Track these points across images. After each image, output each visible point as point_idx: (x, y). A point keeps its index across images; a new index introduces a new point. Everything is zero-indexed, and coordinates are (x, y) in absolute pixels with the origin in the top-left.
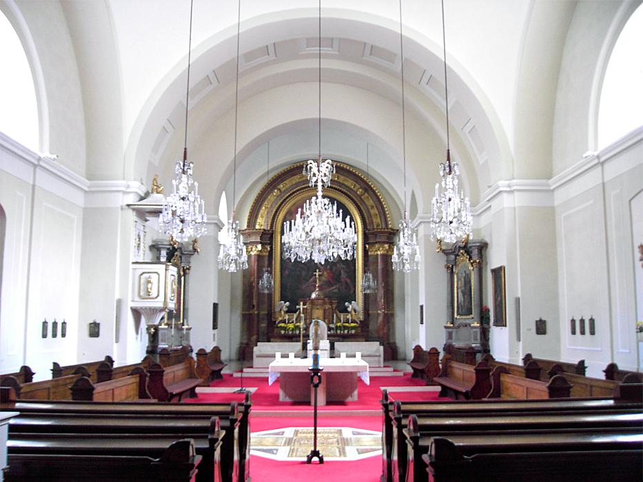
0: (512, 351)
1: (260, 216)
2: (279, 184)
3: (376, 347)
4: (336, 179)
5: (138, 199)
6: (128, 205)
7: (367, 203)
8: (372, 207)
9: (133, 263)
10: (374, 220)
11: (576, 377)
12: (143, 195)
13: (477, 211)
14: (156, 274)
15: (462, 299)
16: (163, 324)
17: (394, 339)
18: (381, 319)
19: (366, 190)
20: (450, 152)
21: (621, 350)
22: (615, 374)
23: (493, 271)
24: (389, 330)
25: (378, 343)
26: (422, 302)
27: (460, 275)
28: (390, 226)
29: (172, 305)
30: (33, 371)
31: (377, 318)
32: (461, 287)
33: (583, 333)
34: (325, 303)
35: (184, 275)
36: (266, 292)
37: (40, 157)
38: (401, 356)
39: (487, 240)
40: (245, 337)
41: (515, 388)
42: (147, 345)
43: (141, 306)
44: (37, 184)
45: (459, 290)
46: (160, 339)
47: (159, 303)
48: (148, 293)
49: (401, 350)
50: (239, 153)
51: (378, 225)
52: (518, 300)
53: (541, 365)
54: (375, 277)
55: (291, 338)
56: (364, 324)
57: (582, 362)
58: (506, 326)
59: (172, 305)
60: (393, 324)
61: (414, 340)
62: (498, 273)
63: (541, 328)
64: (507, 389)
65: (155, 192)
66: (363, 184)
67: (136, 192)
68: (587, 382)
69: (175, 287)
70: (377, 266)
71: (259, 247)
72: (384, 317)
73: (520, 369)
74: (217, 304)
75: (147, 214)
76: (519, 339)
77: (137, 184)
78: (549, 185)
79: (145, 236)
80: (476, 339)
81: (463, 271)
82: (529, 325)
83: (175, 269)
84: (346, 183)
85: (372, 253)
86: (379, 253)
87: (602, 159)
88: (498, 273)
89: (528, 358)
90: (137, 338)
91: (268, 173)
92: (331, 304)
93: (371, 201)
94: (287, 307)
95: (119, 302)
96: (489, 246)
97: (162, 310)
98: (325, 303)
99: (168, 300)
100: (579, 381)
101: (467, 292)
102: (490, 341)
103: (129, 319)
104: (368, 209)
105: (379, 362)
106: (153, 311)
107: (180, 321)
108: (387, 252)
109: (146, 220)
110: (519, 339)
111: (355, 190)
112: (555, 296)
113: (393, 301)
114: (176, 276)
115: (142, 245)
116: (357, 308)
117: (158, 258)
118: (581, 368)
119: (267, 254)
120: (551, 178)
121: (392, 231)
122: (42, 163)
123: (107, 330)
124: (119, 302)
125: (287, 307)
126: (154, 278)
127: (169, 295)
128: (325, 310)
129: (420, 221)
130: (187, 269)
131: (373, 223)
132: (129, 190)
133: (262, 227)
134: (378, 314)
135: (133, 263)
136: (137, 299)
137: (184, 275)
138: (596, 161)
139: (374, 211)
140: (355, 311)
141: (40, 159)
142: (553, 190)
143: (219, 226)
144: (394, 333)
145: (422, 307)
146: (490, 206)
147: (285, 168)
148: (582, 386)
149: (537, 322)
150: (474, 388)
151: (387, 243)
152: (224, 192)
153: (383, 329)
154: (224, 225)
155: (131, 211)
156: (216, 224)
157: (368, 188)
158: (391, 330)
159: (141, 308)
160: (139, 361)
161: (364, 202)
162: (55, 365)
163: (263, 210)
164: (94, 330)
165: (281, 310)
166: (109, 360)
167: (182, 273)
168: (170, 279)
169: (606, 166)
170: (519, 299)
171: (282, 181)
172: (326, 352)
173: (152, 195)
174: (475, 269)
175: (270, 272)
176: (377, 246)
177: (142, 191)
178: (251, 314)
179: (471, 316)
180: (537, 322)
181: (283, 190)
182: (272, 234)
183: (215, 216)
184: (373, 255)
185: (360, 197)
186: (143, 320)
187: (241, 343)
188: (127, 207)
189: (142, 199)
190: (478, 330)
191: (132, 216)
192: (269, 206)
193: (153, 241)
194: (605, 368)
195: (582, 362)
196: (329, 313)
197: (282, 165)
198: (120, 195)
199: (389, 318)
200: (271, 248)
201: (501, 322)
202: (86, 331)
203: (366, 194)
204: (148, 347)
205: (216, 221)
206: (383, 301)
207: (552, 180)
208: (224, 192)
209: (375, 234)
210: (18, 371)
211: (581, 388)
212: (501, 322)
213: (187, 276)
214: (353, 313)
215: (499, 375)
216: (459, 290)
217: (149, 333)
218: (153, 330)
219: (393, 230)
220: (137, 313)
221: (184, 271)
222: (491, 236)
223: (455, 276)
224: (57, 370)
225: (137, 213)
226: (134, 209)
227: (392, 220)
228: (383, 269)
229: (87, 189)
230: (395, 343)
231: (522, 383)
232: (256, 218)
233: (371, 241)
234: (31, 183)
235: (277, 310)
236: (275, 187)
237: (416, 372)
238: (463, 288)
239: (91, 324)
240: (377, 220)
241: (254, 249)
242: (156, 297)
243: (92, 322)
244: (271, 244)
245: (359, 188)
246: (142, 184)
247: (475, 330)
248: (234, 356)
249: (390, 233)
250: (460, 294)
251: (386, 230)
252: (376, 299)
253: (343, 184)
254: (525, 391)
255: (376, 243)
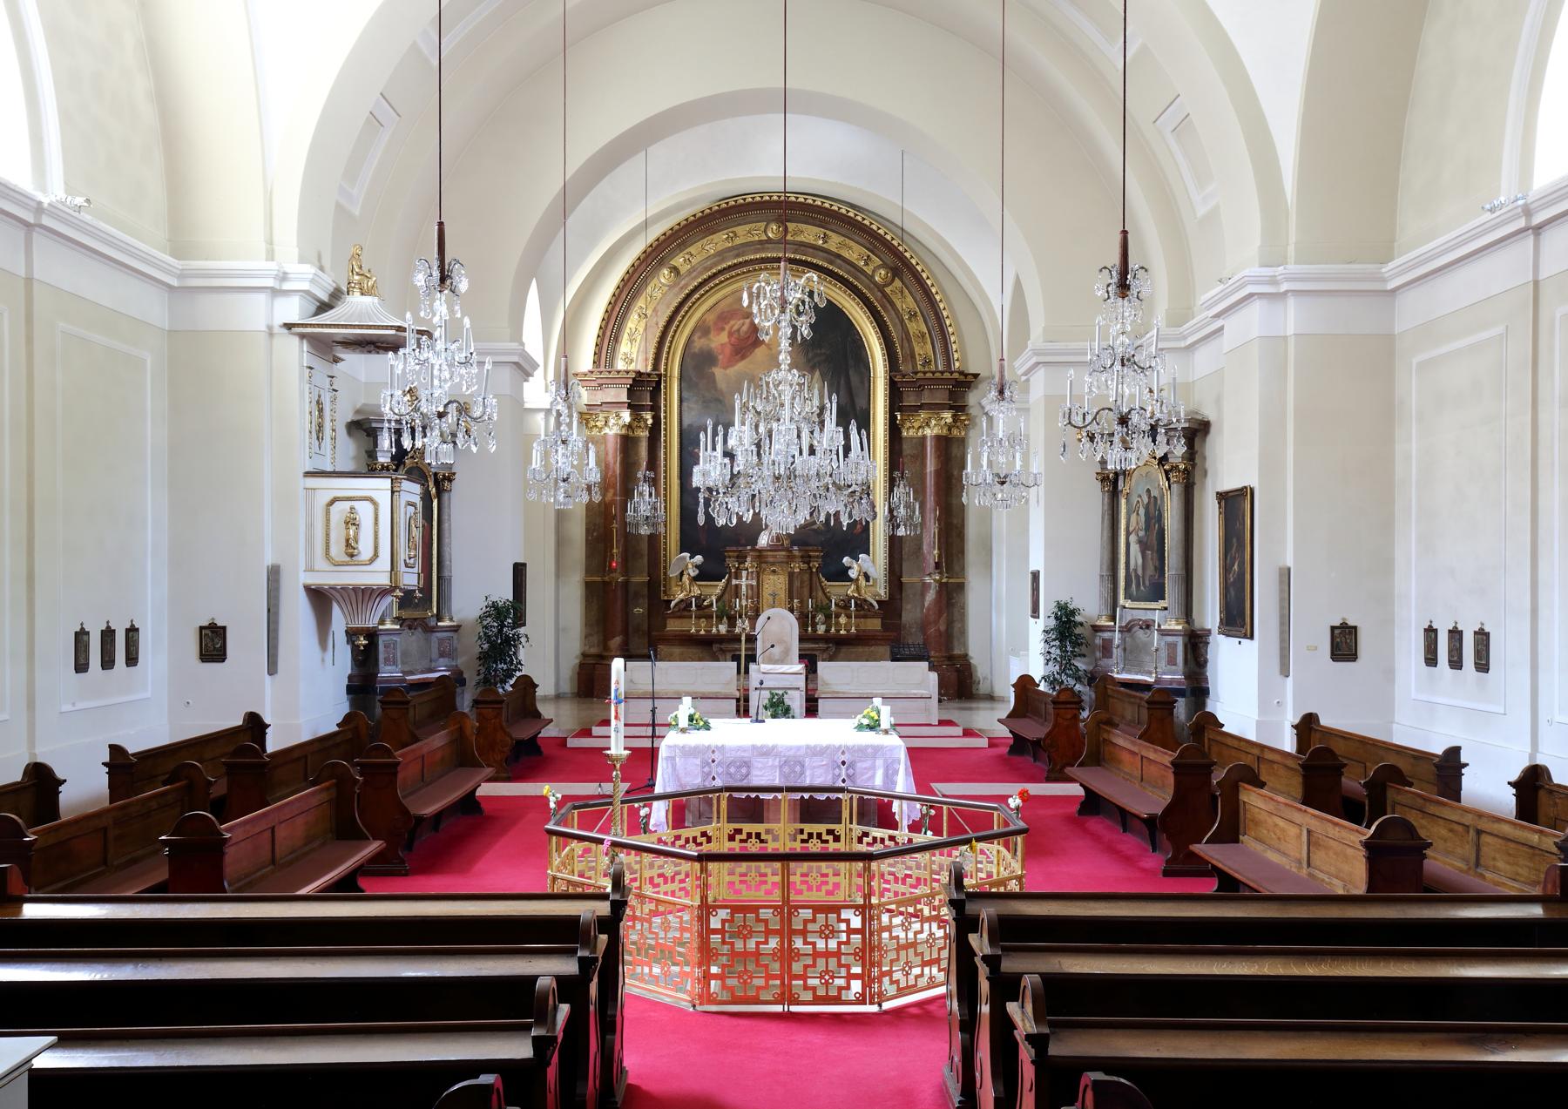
0: (1268, 701)
1: (626, 336)
2: (672, 254)
3: (920, 678)
4: (821, 242)
5: (313, 309)
6: (289, 326)
7: (899, 305)
8: (913, 316)
9: (308, 474)
10: (917, 349)
11: (1444, 804)
12: (325, 298)
13: (1185, 338)
14: (367, 504)
15: (1140, 561)
16: (388, 621)
17: (965, 645)
18: (931, 596)
19: (896, 273)
20: (1129, 236)
21: (1558, 718)
22: (1542, 793)
23: (1223, 497)
24: (950, 623)
25: (925, 665)
26: (1037, 562)
27: (1135, 499)
28: (957, 364)
29: (410, 579)
30: (60, 775)
31: (923, 595)
32: (1136, 531)
33: (1456, 663)
34: (791, 558)
35: (439, 494)
36: (645, 530)
37: (40, 203)
38: (983, 688)
39: (1209, 413)
40: (595, 639)
41: (1276, 825)
42: (349, 672)
43: (332, 582)
44: (36, 276)
45: (1133, 538)
46: (381, 657)
47: (378, 575)
48: (350, 547)
49: (981, 668)
50: (570, 178)
51: (927, 363)
52: (1285, 574)
53: (1339, 748)
54: (920, 493)
55: (709, 647)
56: (890, 608)
57: (1454, 752)
58: (1252, 637)
59: (410, 579)
60: (963, 608)
61: (1015, 652)
62: (1236, 504)
63: (1344, 643)
64: (1257, 823)
65: (357, 293)
66: (890, 259)
67: (307, 292)
68: (1468, 819)
69: (417, 534)
70: (924, 465)
71: (626, 416)
72: (939, 593)
73: (1291, 763)
74: (524, 565)
75: (339, 348)
76: (1285, 671)
77: (309, 270)
78: (1385, 280)
79: (333, 401)
80: (1172, 661)
81: (1142, 491)
82: (1312, 638)
83: (416, 488)
84: (845, 254)
85: (912, 433)
86: (928, 432)
87: (1538, 219)
88: (1236, 504)
89: (1307, 726)
90: (323, 660)
91: (646, 225)
92: (806, 559)
93: (910, 299)
94: (697, 567)
95: (274, 574)
96: (1213, 430)
97: (384, 592)
98: (791, 558)
99: (402, 568)
100: (1446, 813)
101: (1154, 543)
102: (1209, 666)
103: (298, 612)
104: (902, 321)
105: (927, 710)
106: (364, 595)
107: (431, 608)
108: (950, 430)
109: (336, 360)
110: (1285, 671)
111: (868, 270)
112: (1384, 566)
113: (962, 552)
114: (419, 504)
115: (328, 426)
116: (872, 572)
117: (372, 454)
118: (1449, 767)
119: (647, 433)
120: (1392, 259)
121: (962, 378)
122: (46, 221)
123: (245, 644)
124: (274, 574)
125: (697, 567)
126: (364, 511)
127: (403, 554)
128: (791, 575)
129: (1034, 360)
130: (445, 478)
131: (913, 356)
132: (286, 286)
133: (632, 367)
134: (925, 587)
135: (308, 474)
136: (320, 563)
137: (439, 494)
138: (1521, 223)
139: (916, 327)
140: (867, 577)
141: (39, 209)
142: (1394, 291)
143: (524, 369)
144: (963, 632)
145: (1035, 576)
146: (1221, 328)
147: (686, 213)
148: (1456, 827)
149: (1333, 628)
150: (1168, 810)
151: (951, 408)
152: (534, 282)
153: (936, 622)
154: (535, 366)
155: (296, 340)
156: (516, 364)
157: (901, 268)
158: (957, 625)
159: (333, 588)
160: (331, 727)
161: (892, 304)
162: (116, 750)
163: (633, 323)
164: (213, 643)
165: (682, 574)
166: (255, 725)
167: (434, 491)
168: (404, 513)
169: (1548, 236)
170: (1289, 569)
171: (683, 246)
172: (797, 692)
173: (349, 298)
174: (1174, 487)
175: (654, 482)
176: (923, 415)
177: (323, 288)
178: (609, 583)
179: (1162, 604)
180: (1333, 628)
181: (684, 269)
182: (659, 383)
183: (514, 345)
184: (912, 438)
185: (881, 288)
186: (336, 612)
187: (584, 655)
188: (285, 331)
189: (323, 307)
190: (1180, 641)
191: (294, 352)
192: (649, 312)
193: (358, 412)
194: (1514, 777)
195: (1454, 752)
196: (802, 582)
197: (679, 207)
198: (262, 298)
199: (952, 595)
200: (656, 419)
201: (1237, 620)
202: (192, 646)
203: (898, 283)
204: (350, 678)
205: (515, 359)
206: (936, 552)
207: (1391, 265)
208: (534, 282)
209: (919, 386)
210: (18, 778)
211: (1451, 830)
212: (1237, 620)
213: (445, 496)
214: (862, 582)
215: (1235, 790)
216: (1133, 538)
217: (355, 649)
218: (363, 641)
219: (966, 375)
220: (320, 598)
221: (437, 483)
222: (1218, 401)
223: (1123, 501)
224: (120, 764)
225: (309, 342)
226: (302, 336)
227: (963, 349)
228: (938, 473)
229: (175, 282)
230: (965, 656)
231: (1298, 817)
232: (616, 339)
233: (909, 401)
234: (22, 272)
235: (673, 573)
236: (661, 263)
237: (1020, 744)
238: (1142, 533)
239: (201, 628)
240: (923, 350)
241: (612, 421)
242: (372, 561)
243: (206, 624)
244: (655, 409)
245: (879, 267)
246: (322, 269)
247: (1170, 639)
248: (567, 687)
249: (958, 384)
250: (1135, 548)
251: (947, 375)
252: (919, 547)
253: (839, 256)
254: (1305, 838)
255: (921, 407)
